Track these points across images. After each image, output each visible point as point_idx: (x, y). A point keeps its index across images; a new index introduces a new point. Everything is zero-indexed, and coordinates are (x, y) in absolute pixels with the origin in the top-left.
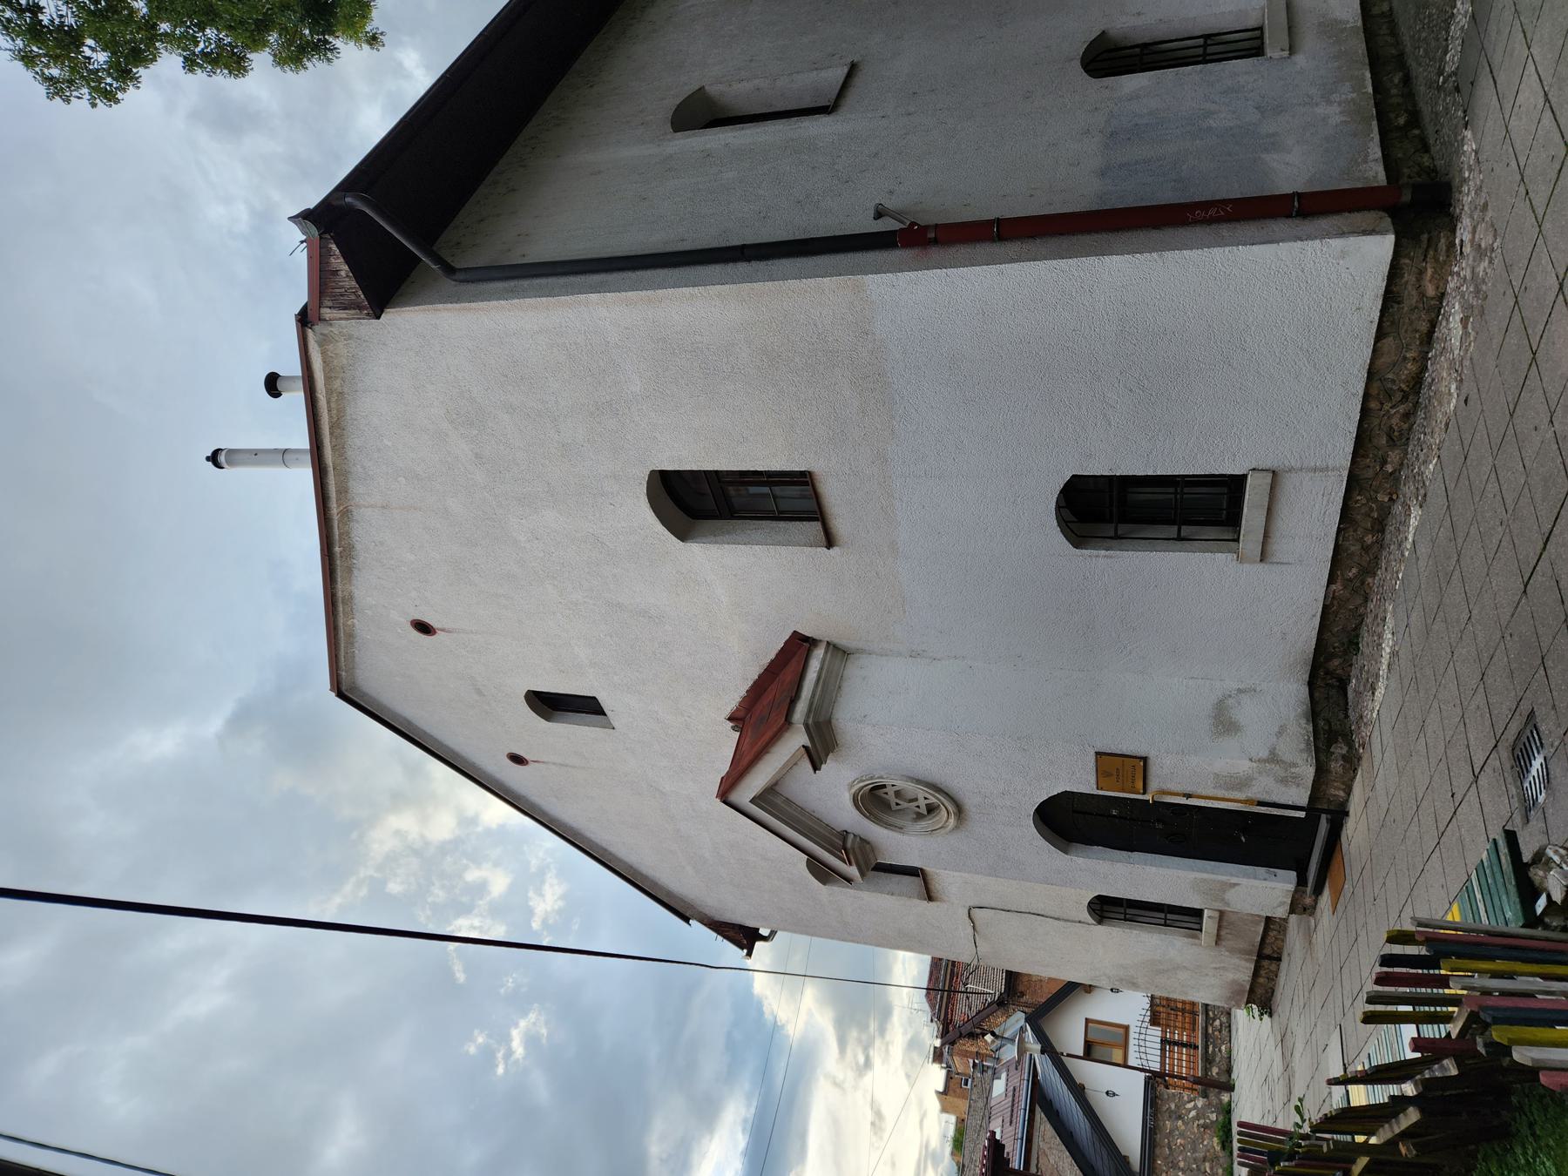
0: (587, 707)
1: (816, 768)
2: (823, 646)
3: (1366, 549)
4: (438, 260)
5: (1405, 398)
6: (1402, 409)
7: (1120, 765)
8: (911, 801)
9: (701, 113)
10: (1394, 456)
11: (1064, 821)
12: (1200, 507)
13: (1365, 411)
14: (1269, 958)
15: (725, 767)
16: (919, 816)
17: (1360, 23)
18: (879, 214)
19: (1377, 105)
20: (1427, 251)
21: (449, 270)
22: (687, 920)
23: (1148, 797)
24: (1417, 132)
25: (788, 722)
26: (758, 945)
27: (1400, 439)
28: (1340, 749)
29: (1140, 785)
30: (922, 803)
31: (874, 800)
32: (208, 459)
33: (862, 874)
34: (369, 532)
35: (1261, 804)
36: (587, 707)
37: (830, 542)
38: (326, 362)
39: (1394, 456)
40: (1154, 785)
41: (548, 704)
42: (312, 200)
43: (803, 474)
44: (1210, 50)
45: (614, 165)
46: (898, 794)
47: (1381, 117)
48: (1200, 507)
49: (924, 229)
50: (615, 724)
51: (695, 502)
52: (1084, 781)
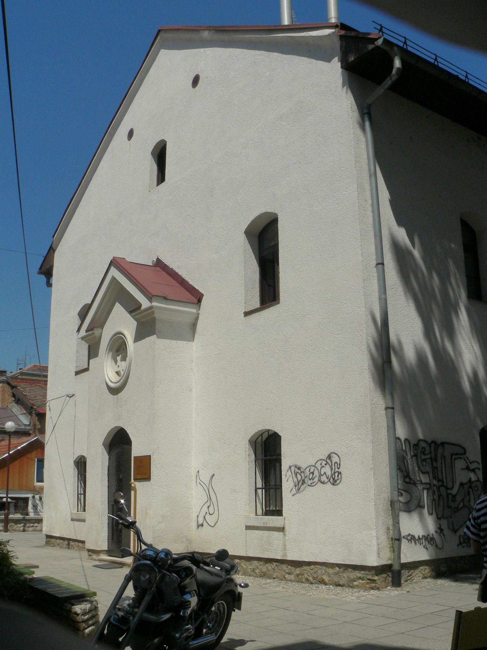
5: (314, 578)
11: (119, 442)
12: (271, 498)
14: (69, 544)
23: (132, 481)
33: (83, 338)
37: (247, 314)
39: (292, 577)
41: (160, 155)
48: (271, 498)
52: (137, 450)
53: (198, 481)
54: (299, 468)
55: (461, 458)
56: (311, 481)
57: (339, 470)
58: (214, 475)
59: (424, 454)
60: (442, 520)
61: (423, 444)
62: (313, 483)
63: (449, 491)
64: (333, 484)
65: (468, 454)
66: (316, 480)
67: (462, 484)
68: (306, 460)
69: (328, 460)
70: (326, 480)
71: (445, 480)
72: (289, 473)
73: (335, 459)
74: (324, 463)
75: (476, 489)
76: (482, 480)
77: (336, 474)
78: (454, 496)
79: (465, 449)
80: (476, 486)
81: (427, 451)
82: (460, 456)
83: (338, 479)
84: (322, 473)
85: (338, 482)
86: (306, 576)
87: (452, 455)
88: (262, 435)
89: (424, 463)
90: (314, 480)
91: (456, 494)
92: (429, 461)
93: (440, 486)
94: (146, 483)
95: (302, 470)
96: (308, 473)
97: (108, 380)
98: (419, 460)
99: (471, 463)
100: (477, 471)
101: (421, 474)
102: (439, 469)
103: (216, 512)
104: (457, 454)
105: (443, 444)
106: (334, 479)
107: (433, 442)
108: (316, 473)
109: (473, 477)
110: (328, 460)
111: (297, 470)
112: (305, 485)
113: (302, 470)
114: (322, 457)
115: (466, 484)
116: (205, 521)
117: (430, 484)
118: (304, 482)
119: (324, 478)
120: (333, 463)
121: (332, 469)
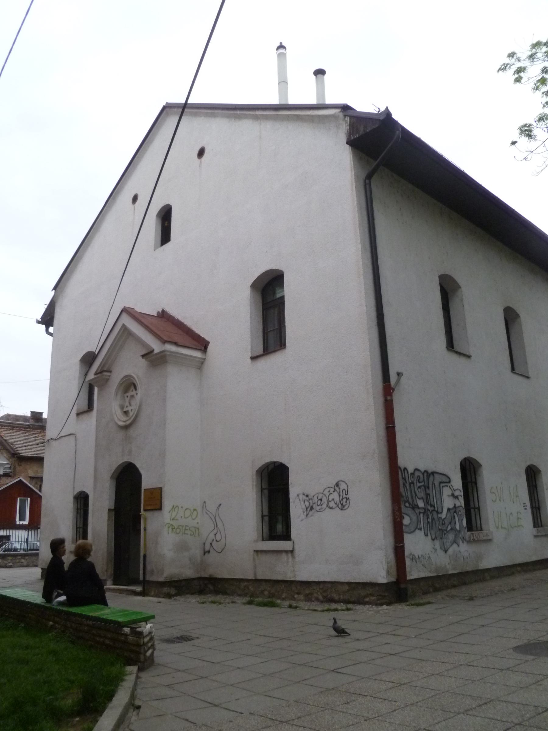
0: (165, 236)
1: (143, 356)
2: (204, 357)
3: (262, 592)
4: (377, 166)
5: (324, 597)
6: (321, 597)
7: (156, 499)
8: (130, 403)
9: (448, 290)
10: (302, 597)
11: (127, 478)
12: (276, 518)
13: (319, 583)
15: (139, 309)
16: (122, 407)
17: (481, 568)
18: (399, 374)
19: (443, 575)
20: (380, 596)
21: (369, 177)
22: (55, 288)
23: (142, 512)
24: (431, 590)
25: (164, 342)
26: (43, 327)
27: (309, 598)
28: (173, 591)
29: (149, 508)
30: (129, 408)
31: (129, 385)
32: (281, 43)
34: (247, 127)
35: (145, 556)
36: (165, 236)
37: (253, 358)
38: (326, 116)
39: (302, 597)
40: (148, 514)
42: (395, 116)
43: (285, 345)
44: (472, 511)
45: (420, 252)
46: (132, 396)
47: (438, 577)
48: (276, 518)
49: (391, 395)
50: (157, 250)
51: (269, 289)
52: (147, 483)
53: (205, 510)
54: (307, 496)
55: (447, 486)
56: (320, 507)
57: (347, 497)
58: (221, 505)
59: (419, 482)
60: (436, 541)
61: (417, 474)
62: (322, 508)
63: (439, 515)
64: (342, 509)
65: (452, 483)
66: (324, 506)
67: (449, 509)
68: (314, 489)
69: (336, 488)
70: (334, 506)
71: (436, 506)
72: (297, 500)
73: (343, 486)
74: (332, 490)
75: (460, 513)
76: (463, 506)
77: (345, 500)
78: (443, 520)
79: (449, 478)
80: (459, 511)
81: (421, 480)
82: (446, 484)
83: (346, 505)
84: (330, 500)
85: (346, 507)
86: (315, 595)
87: (440, 483)
88: (268, 466)
89: (419, 490)
90: (323, 506)
91: (444, 519)
92: (423, 488)
93: (432, 511)
94: (293, 478)
95: (310, 497)
96: (316, 500)
97: (116, 419)
98: (415, 487)
99: (455, 491)
100: (460, 497)
101: (417, 499)
102: (431, 495)
103: (223, 539)
104: (444, 482)
105: (433, 473)
106: (342, 504)
107: (425, 471)
108: (324, 500)
109: (458, 504)
110: (336, 488)
111: (305, 498)
112: (313, 511)
113: (310, 497)
114: (330, 486)
115: (452, 509)
116: (212, 548)
117: (424, 509)
118: (312, 508)
119: (332, 504)
120: (341, 490)
121: (340, 496)
